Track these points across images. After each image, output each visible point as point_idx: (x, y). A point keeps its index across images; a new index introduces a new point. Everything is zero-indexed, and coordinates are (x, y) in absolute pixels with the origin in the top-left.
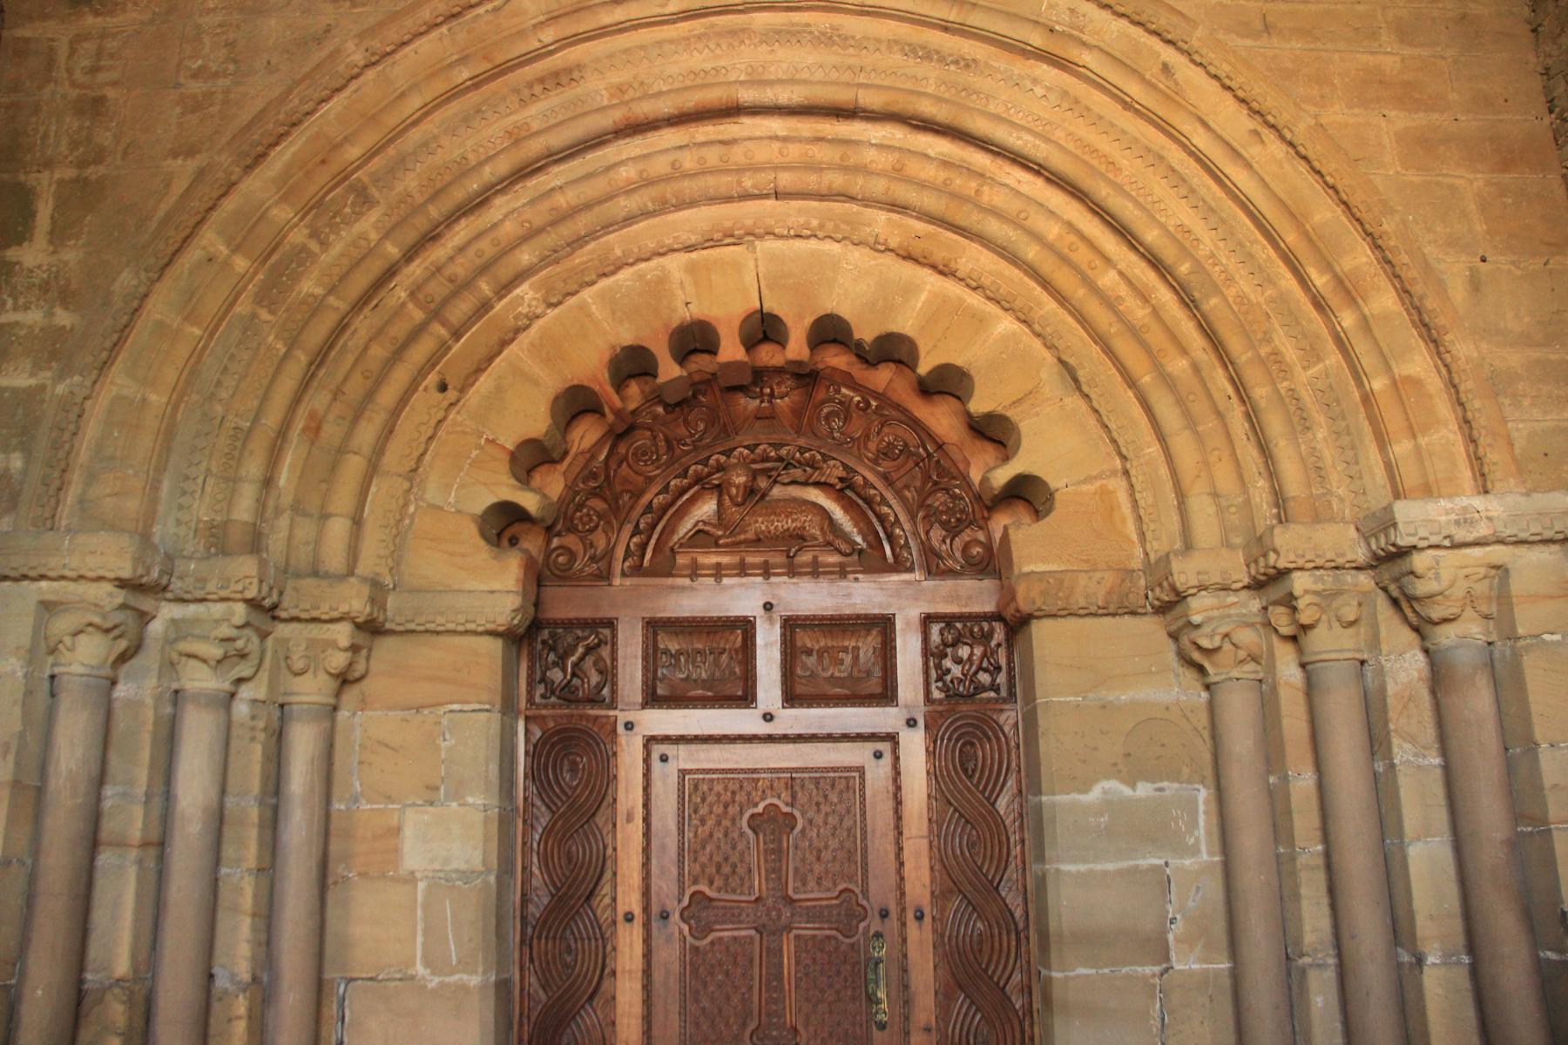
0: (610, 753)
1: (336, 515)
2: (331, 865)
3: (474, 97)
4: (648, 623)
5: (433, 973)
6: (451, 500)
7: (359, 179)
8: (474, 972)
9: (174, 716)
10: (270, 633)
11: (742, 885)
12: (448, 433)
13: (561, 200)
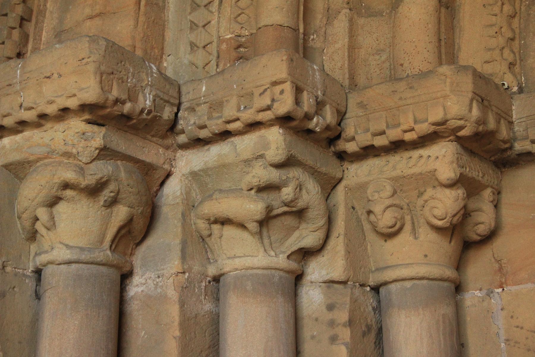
10: (340, 180)
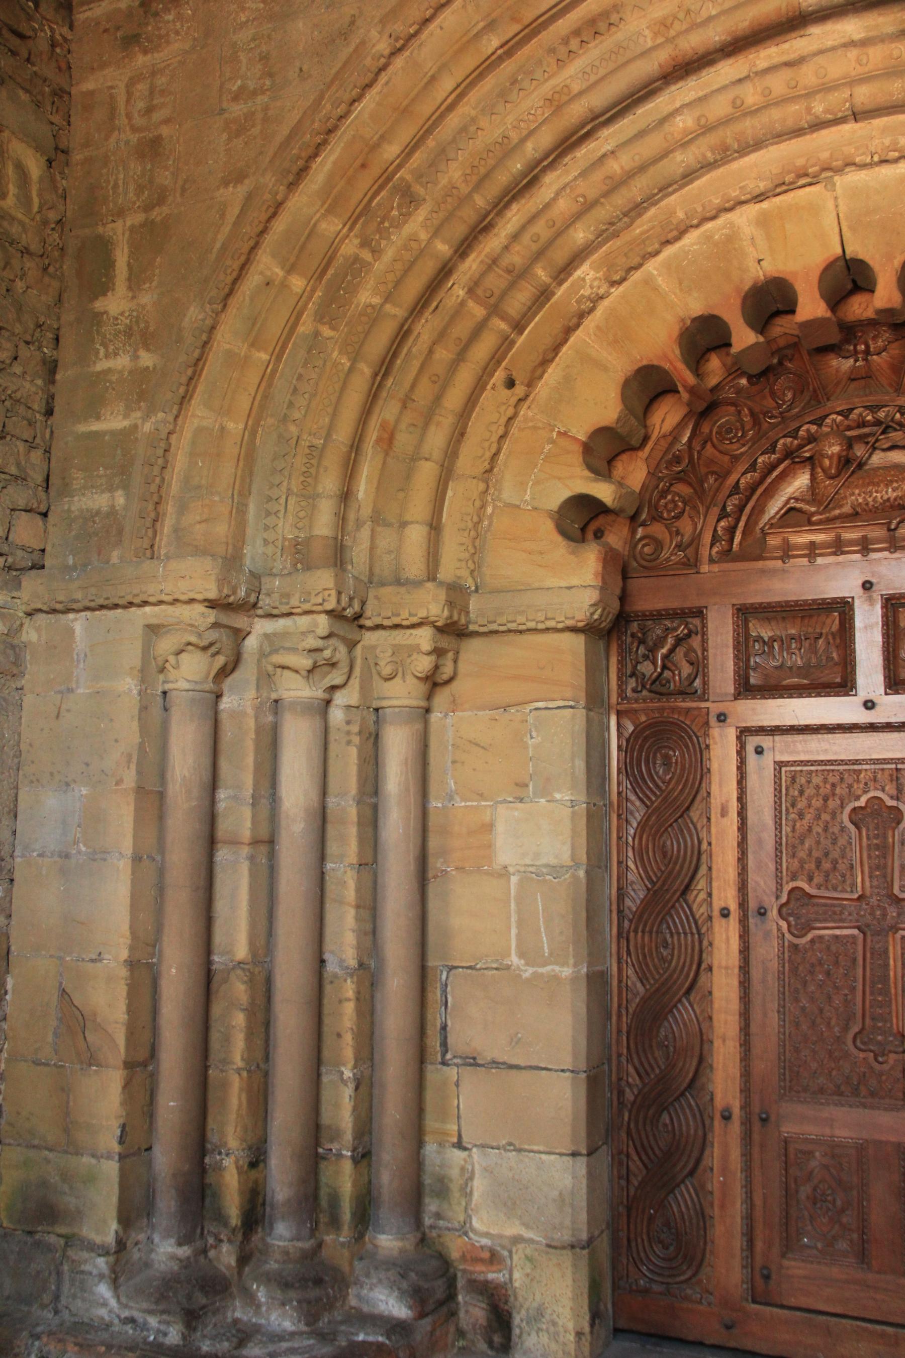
0: (703, 746)
1: (412, 523)
2: (431, 860)
3: (508, 67)
4: (739, 610)
5: (527, 964)
6: (527, 497)
7: (402, 179)
8: (564, 964)
9: (276, 723)
11: (844, 882)
12: (521, 430)
13: (615, 167)
